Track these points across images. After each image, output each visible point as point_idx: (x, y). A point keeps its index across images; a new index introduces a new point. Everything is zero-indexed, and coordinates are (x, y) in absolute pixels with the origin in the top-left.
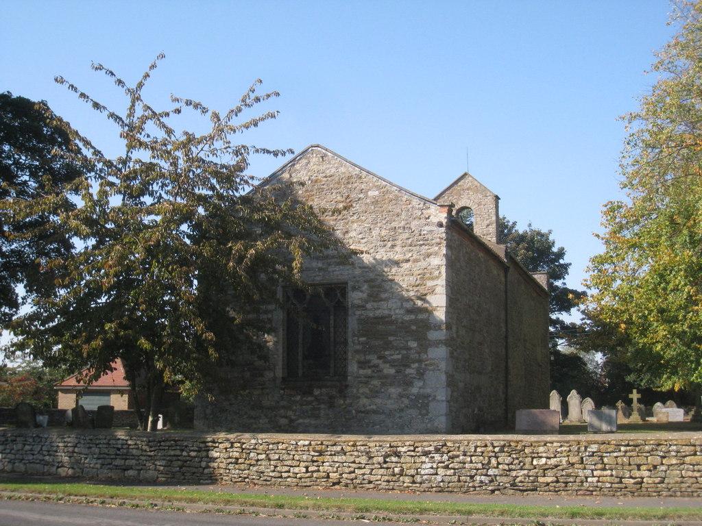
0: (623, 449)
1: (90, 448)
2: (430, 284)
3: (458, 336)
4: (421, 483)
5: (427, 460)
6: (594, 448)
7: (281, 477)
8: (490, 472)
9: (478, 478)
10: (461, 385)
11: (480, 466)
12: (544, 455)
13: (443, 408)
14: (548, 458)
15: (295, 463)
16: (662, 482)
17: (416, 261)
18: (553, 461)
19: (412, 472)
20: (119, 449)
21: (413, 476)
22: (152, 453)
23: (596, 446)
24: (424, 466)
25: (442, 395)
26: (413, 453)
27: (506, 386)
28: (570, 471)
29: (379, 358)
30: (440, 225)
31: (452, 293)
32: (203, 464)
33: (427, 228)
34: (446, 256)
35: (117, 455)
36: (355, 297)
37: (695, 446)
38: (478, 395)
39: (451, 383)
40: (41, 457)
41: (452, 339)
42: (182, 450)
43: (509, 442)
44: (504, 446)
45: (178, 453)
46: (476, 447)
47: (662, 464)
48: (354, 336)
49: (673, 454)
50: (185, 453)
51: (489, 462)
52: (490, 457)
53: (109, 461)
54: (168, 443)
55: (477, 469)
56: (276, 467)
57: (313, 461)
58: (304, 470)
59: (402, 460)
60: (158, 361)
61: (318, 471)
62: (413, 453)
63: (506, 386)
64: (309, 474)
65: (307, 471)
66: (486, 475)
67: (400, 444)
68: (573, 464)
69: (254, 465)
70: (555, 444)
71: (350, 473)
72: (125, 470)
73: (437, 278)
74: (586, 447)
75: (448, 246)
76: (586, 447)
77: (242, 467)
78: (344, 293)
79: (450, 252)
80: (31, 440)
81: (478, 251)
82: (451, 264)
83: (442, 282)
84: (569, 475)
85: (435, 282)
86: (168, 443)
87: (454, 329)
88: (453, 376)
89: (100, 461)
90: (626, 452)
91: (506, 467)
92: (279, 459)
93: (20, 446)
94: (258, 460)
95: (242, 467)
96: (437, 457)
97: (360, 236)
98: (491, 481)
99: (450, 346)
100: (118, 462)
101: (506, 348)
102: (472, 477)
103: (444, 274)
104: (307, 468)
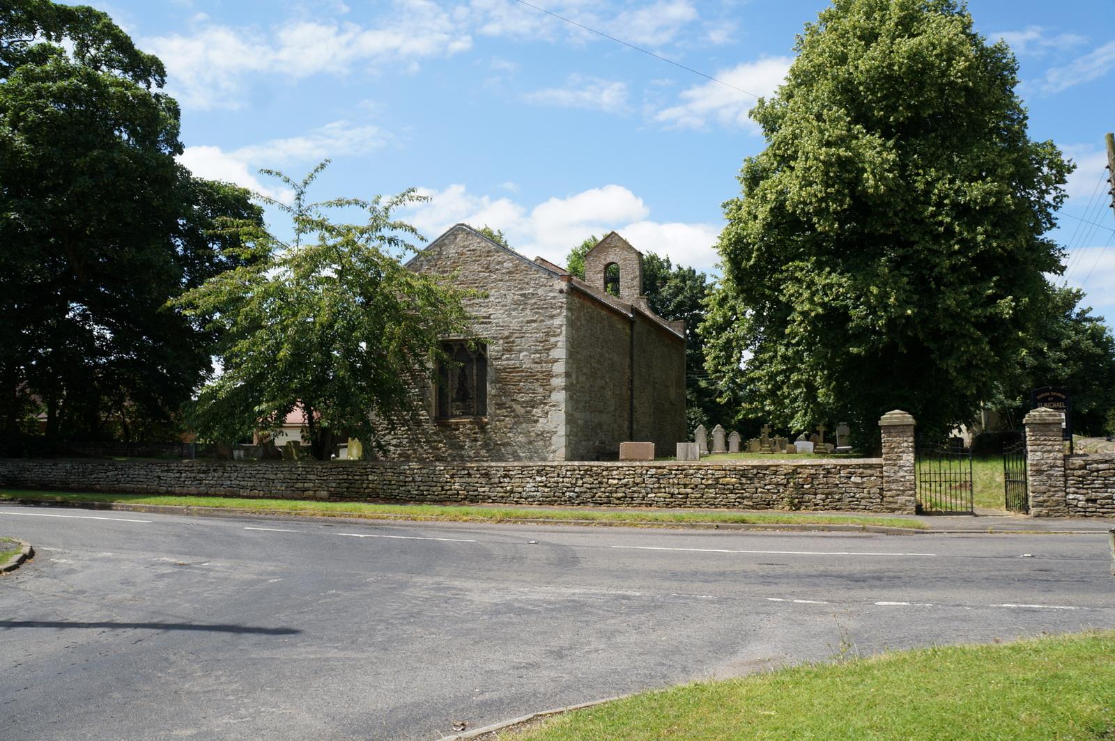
0: (673, 472)
1: (277, 474)
2: (553, 340)
3: (578, 383)
4: (526, 499)
5: (531, 481)
6: (653, 471)
7: (423, 494)
8: (577, 489)
9: (567, 494)
10: (580, 422)
11: (569, 485)
12: (616, 477)
13: (563, 441)
14: (619, 479)
15: (433, 484)
16: (701, 497)
17: (543, 321)
18: (624, 481)
19: (520, 489)
20: (299, 475)
21: (520, 493)
22: (325, 478)
23: (654, 470)
24: (528, 485)
25: (562, 430)
26: (521, 476)
27: (631, 423)
28: (635, 489)
29: (513, 400)
30: (561, 291)
31: (572, 347)
32: (364, 486)
33: (551, 294)
34: (566, 317)
35: (297, 479)
36: (492, 350)
37: (725, 470)
38: (599, 431)
39: (570, 420)
40: (238, 482)
41: (572, 384)
42: (348, 475)
43: (591, 467)
44: (587, 470)
45: (345, 477)
46: (567, 471)
47: (702, 484)
48: (452, 401)
49: (710, 476)
50: (350, 477)
51: (576, 482)
52: (577, 478)
53: (291, 484)
54: (338, 470)
55: (568, 488)
56: (419, 486)
57: (447, 482)
58: (440, 489)
59: (513, 481)
60: (338, 456)
61: (451, 490)
62: (521, 476)
63: (631, 423)
64: (444, 492)
65: (443, 490)
66: (574, 492)
67: (511, 468)
68: (637, 484)
69: (402, 486)
70: (625, 469)
71: (474, 491)
72: (304, 491)
73: (559, 335)
74: (647, 471)
75: (569, 309)
76: (647, 471)
77: (394, 487)
78: (484, 347)
79: (570, 314)
80: (229, 469)
81: (599, 310)
82: (571, 323)
83: (562, 338)
84: (634, 492)
85: (557, 339)
86: (338, 470)
87: (574, 376)
88: (572, 415)
89: (284, 485)
90: (676, 474)
91: (589, 486)
92: (421, 481)
93: (220, 474)
94: (406, 482)
95: (394, 487)
96: (538, 479)
97: (497, 300)
98: (578, 497)
99: (570, 390)
100: (299, 485)
101: (631, 390)
102: (563, 493)
103: (564, 332)
104: (442, 487)
